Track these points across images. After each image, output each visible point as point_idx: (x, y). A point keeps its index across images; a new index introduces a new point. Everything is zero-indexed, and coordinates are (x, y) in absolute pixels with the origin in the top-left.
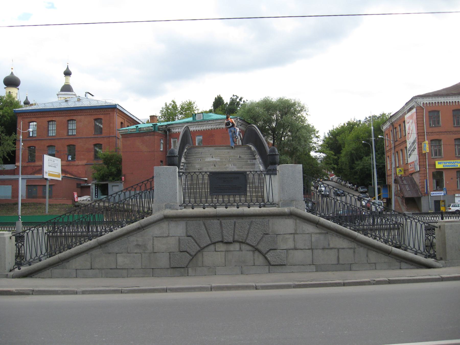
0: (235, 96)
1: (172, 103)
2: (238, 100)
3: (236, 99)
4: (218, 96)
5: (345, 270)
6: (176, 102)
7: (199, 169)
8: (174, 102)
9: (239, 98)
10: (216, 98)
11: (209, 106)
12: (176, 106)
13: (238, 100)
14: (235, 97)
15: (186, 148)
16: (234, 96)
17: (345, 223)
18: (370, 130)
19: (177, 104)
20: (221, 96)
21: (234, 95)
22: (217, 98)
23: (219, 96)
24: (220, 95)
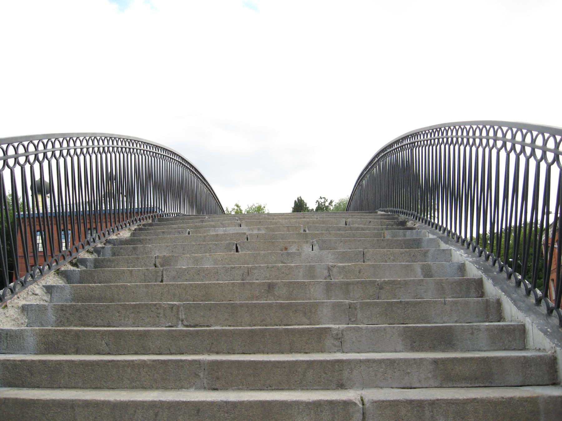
0: (323, 198)
1: (236, 208)
2: (327, 204)
3: (324, 202)
4: (298, 199)
5: (10, 386)
6: (240, 207)
7: (158, 264)
8: (237, 206)
9: (329, 201)
10: (295, 202)
11: (288, 208)
12: (241, 210)
13: (327, 204)
14: (323, 200)
15: (51, 279)
16: (321, 198)
17: (170, 324)
18: (522, 325)
19: (242, 208)
20: (237, 204)
21: (322, 197)
22: (297, 201)
23: (299, 198)
24: (300, 197)
